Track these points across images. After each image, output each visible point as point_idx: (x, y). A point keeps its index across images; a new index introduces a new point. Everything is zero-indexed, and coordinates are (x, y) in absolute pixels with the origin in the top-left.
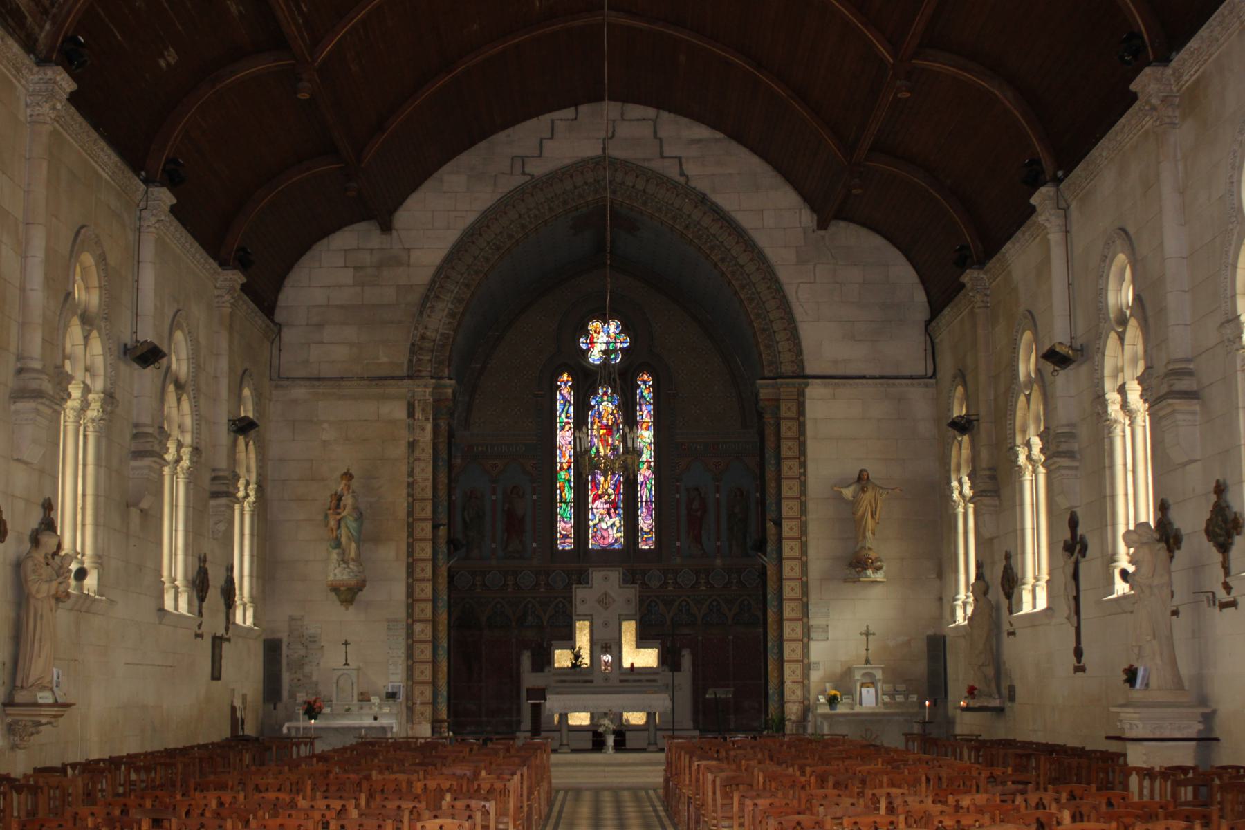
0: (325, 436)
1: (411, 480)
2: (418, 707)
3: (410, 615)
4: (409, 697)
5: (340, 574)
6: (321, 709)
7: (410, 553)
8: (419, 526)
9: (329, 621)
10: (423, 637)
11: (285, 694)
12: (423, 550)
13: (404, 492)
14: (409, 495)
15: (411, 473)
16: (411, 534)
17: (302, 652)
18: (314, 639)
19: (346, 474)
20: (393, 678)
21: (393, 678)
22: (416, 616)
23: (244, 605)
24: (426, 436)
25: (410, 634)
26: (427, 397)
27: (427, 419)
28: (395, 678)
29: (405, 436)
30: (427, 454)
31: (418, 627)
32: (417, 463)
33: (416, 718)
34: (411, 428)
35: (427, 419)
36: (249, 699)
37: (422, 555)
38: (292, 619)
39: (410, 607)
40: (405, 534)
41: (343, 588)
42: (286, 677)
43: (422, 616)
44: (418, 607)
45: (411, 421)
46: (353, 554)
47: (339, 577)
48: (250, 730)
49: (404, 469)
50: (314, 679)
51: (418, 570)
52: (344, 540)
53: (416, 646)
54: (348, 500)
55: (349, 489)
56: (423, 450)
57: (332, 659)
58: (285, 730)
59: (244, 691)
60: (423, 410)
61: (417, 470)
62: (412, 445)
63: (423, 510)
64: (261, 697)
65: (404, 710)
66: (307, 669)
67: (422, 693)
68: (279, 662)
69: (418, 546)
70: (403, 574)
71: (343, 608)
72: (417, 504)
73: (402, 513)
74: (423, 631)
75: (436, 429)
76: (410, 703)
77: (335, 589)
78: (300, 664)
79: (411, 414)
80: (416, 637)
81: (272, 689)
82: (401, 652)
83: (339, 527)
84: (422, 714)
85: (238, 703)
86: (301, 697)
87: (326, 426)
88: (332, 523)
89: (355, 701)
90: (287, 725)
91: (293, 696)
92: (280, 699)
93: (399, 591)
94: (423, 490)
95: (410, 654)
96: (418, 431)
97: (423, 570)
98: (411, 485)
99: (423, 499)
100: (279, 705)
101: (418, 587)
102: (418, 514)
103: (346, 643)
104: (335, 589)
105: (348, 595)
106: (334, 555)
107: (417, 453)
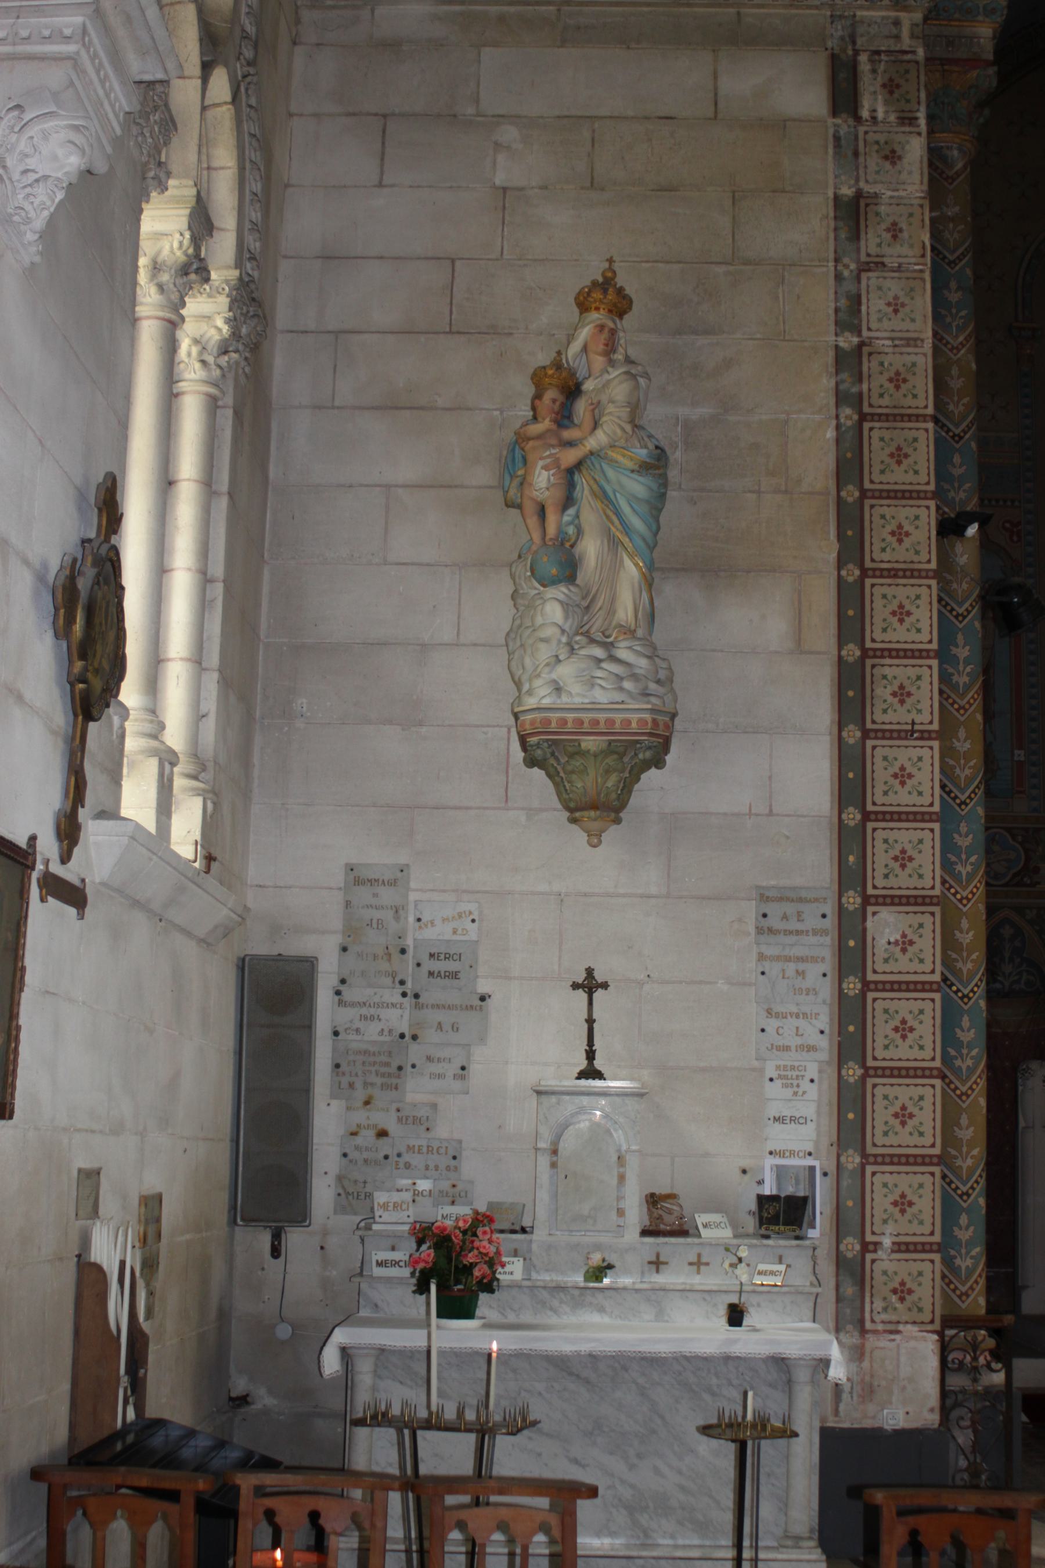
0: (504, 172)
1: (848, 341)
2: (885, 1264)
3: (851, 873)
4: (849, 1221)
5: (576, 687)
6: (493, 1262)
7: (851, 619)
8: (882, 520)
9: (524, 894)
10: (904, 966)
11: (322, 1193)
12: (901, 613)
13: (823, 385)
14: (841, 398)
15: (849, 316)
16: (852, 546)
17: (399, 1019)
18: (448, 965)
19: (606, 283)
20: (781, 1137)
21: (781, 1137)
22: (878, 882)
23: (167, 759)
24: (904, 185)
25: (851, 956)
26: (906, 42)
27: (907, 120)
28: (792, 1135)
29: (825, 179)
30: (912, 250)
31: (885, 926)
32: (870, 279)
33: (874, 1308)
34: (849, 153)
35: (907, 120)
36: (170, 1214)
37: (900, 635)
38: (357, 878)
39: (851, 843)
40: (828, 550)
41: (590, 743)
42: (328, 1121)
43: (903, 882)
44: (884, 843)
45: (844, 125)
46: (625, 611)
47: (577, 695)
48: (170, 1396)
49: (822, 299)
50: (442, 1131)
51: (883, 692)
52: (591, 549)
53: (879, 1004)
54: (608, 387)
55: (610, 348)
56: (895, 231)
57: (527, 1043)
58: (331, 1362)
59: (153, 1182)
60: (890, 87)
61: (874, 306)
62: (853, 213)
63: (899, 456)
64: (223, 1198)
65: (827, 1269)
66: (416, 1091)
67: (903, 1204)
68: (304, 1057)
69: (881, 599)
70: (822, 711)
71: (580, 836)
72: (876, 435)
73: (817, 465)
74: (905, 944)
75: (936, 158)
76: (851, 1246)
77: (546, 748)
78: (383, 1069)
79: (844, 97)
80: (879, 968)
81: (267, 1172)
82: (815, 1026)
83: (568, 501)
84: (902, 1292)
85: (109, 1249)
86: (404, 1202)
87: (509, 134)
88: (542, 481)
89: (632, 1235)
90: (340, 1336)
91: (354, 1196)
92: (301, 1216)
93: (807, 776)
94: (898, 380)
95: (851, 1041)
96: (873, 162)
97: (902, 694)
98: (849, 362)
99: (897, 417)
100: (294, 1238)
101: (883, 759)
102: (882, 471)
103: (590, 985)
104: (546, 748)
105: (596, 774)
106: (552, 610)
107: (872, 242)
